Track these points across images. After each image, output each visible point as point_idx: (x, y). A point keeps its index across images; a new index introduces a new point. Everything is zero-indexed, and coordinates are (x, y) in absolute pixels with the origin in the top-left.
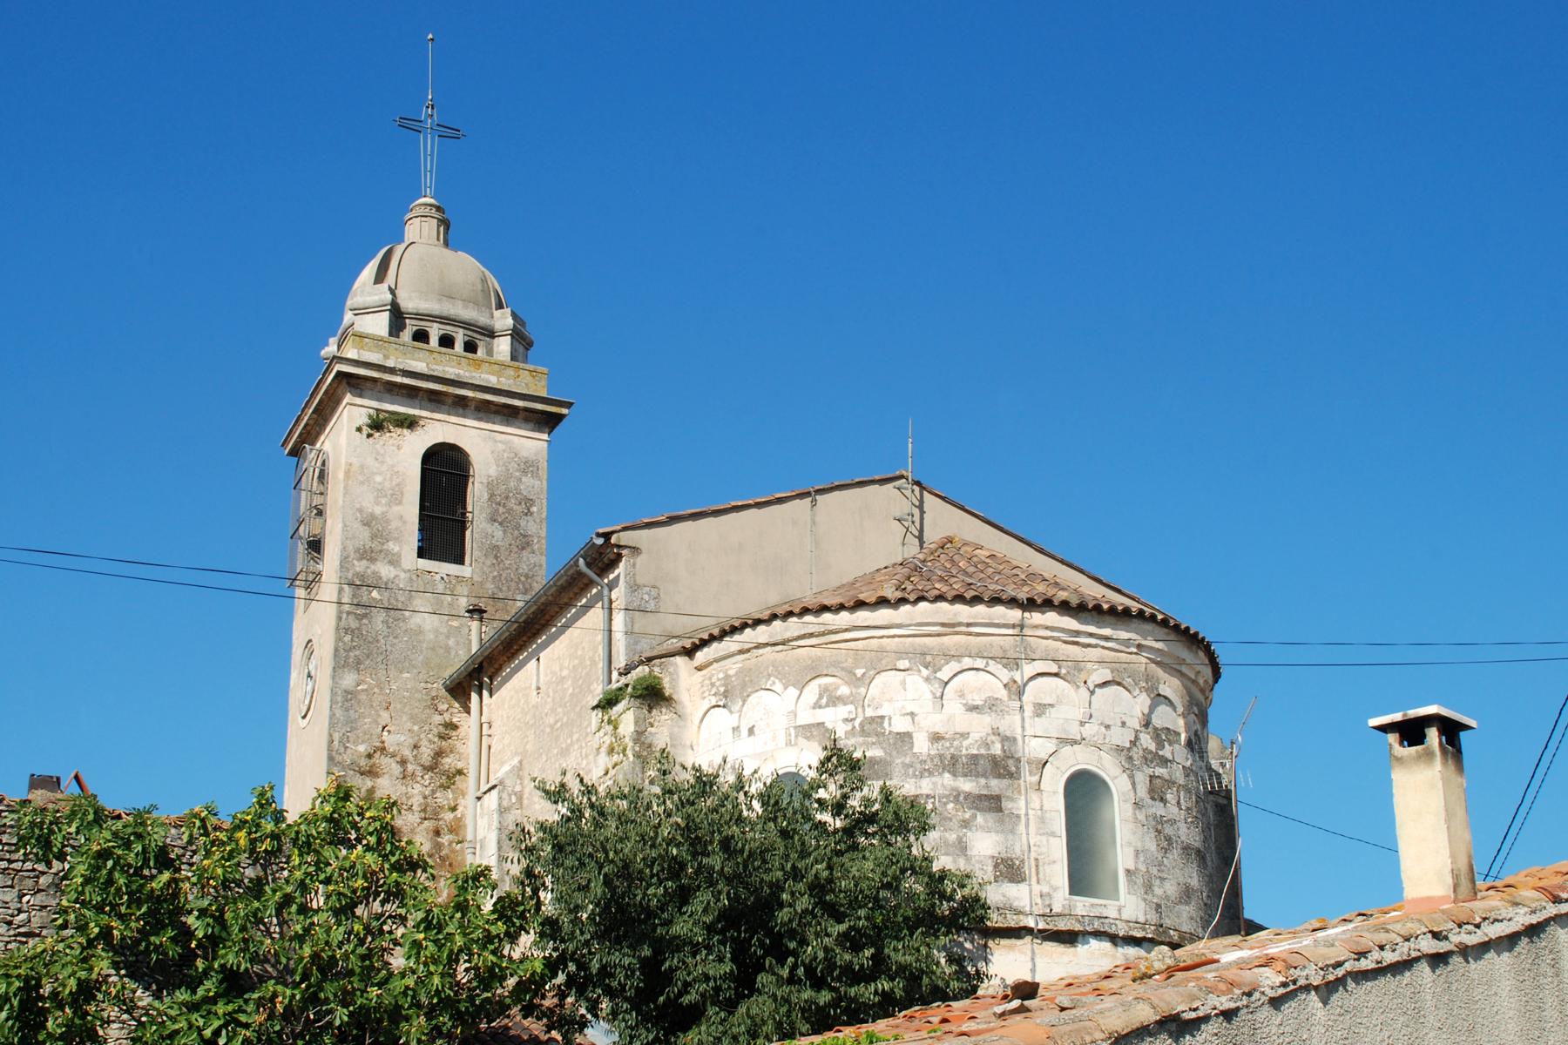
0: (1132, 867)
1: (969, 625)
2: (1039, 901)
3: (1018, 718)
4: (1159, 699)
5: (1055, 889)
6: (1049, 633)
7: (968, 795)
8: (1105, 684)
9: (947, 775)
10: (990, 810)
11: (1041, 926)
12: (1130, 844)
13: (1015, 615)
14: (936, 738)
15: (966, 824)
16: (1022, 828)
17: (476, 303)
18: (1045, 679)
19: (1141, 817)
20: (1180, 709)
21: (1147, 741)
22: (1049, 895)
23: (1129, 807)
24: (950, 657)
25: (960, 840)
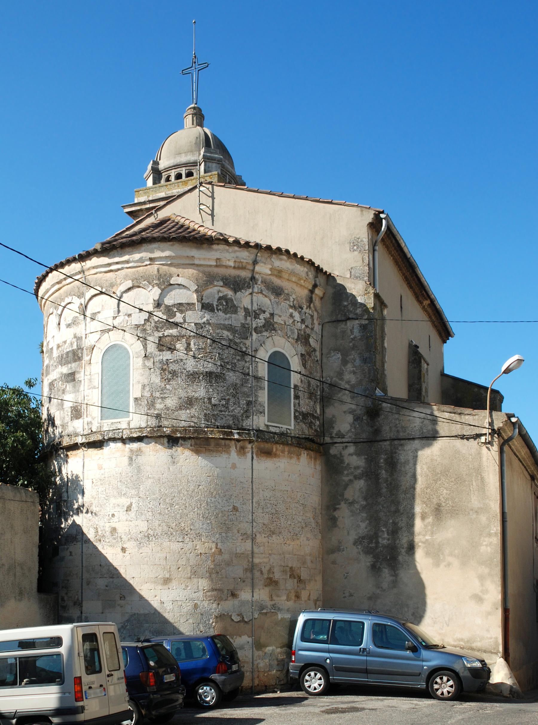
0: (139, 395)
2: (86, 427)
8: (129, 289)
12: (139, 382)
17: (191, 151)
19: (149, 364)
21: (160, 314)
22: (91, 422)
23: (140, 361)
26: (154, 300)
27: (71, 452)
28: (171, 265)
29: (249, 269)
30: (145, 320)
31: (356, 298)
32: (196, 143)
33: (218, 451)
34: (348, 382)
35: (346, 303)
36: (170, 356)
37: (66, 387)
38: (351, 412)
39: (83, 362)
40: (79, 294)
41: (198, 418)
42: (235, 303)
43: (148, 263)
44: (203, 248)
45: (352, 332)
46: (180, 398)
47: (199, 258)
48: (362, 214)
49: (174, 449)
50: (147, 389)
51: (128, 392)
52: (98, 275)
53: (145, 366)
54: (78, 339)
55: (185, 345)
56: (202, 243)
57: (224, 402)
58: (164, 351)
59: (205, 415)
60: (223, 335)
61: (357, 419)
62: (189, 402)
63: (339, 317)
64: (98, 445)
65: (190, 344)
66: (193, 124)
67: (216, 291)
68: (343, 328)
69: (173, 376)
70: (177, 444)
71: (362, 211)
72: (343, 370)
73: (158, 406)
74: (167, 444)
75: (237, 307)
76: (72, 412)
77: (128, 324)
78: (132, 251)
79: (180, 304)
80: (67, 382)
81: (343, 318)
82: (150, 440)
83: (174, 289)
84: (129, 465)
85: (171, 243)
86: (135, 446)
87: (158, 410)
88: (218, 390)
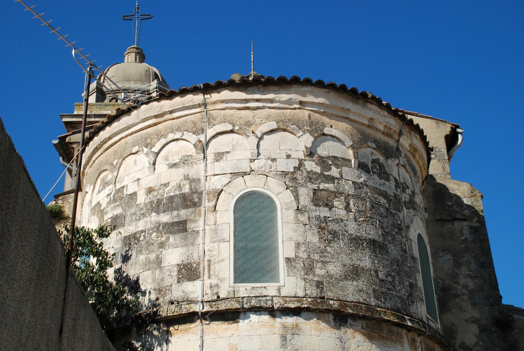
0: (292, 255)
1: (171, 112)
2: (209, 291)
3: (203, 165)
4: (320, 136)
5: (222, 280)
6: (224, 105)
7: (165, 225)
8: (272, 131)
9: (154, 214)
10: (179, 232)
11: (207, 308)
12: (291, 239)
13: (199, 98)
14: (150, 190)
15: (162, 245)
16: (200, 240)
18: (220, 137)
20: (349, 143)
22: (217, 286)
23: (291, 214)
24: (160, 136)
25: (158, 257)
26: (306, 148)
27: (176, 327)
28: (323, 114)
29: (394, 139)
30: (295, 168)
31: (461, 199)
32: (146, 75)
33: (392, 340)
34: (465, 287)
35: (450, 203)
36: (329, 213)
37: (168, 238)
38: (475, 321)
39: (202, 208)
40: (194, 130)
41: (367, 293)
42: (387, 170)
43: (298, 106)
44: (358, 103)
45: (462, 234)
46: (345, 266)
47: (354, 113)
48: (438, 126)
49: (343, 330)
50: (303, 248)
51: (276, 249)
52: (227, 110)
53: (299, 220)
54: (194, 181)
55: (345, 204)
56: (358, 99)
57: (390, 279)
58: (320, 206)
59: (374, 291)
60: (381, 201)
61: (483, 330)
62: (355, 272)
63: (444, 216)
64: (231, 316)
65: (349, 204)
66: (136, 61)
67: (369, 153)
68: (450, 228)
69: (334, 237)
70: (346, 324)
71: (437, 123)
72: (457, 273)
73: (318, 271)
74: (333, 323)
75: (389, 175)
76: (179, 272)
77: (273, 169)
79: (335, 157)
80: (171, 233)
81: (449, 218)
82: (310, 314)
84: (281, 347)
85: (327, 90)
86: (290, 320)
87: (319, 276)
88: (383, 263)
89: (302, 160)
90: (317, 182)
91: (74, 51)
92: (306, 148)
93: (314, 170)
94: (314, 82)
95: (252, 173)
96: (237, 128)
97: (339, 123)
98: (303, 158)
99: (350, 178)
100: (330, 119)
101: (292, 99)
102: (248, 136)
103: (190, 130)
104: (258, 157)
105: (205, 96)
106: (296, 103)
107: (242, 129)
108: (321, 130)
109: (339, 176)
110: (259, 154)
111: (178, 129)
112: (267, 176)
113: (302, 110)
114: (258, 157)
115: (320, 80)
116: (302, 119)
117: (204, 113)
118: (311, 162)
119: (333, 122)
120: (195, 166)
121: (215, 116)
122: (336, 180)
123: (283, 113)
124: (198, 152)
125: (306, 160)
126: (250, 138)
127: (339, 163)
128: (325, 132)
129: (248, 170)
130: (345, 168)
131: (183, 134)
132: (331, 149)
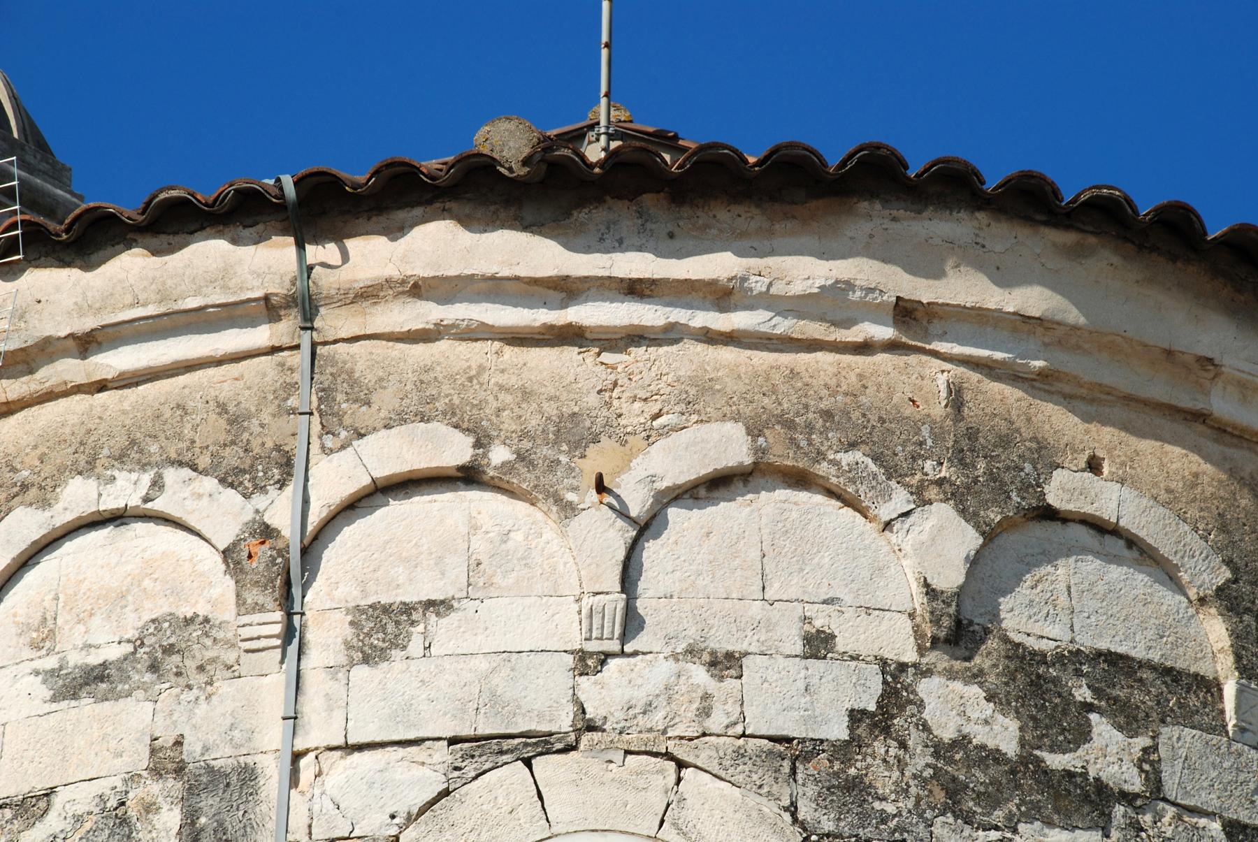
1: (87, 344)
3: (275, 683)
4: (1020, 524)
6: (426, 313)
8: (718, 485)
13: (268, 262)
18: (396, 509)
26: (931, 592)
28: (1041, 384)
30: (856, 716)
40: (232, 457)
43: (885, 332)
47: (1242, 385)
52: (443, 345)
77: (716, 722)
78: (771, 233)
79: (1112, 658)
83: (1069, 551)
85: (1069, 238)
89: (903, 667)
90: (998, 816)
91: (16, 135)
92: (931, 592)
93: (980, 736)
94: (991, 184)
95: (586, 738)
96: (499, 455)
97: (1147, 445)
98: (910, 656)
99: (1209, 800)
100: (1087, 419)
101: (850, 285)
102: (569, 510)
103: (204, 461)
104: (624, 638)
105: (310, 248)
106: (871, 312)
107: (531, 465)
108: (1025, 488)
109: (1135, 783)
110: (632, 623)
111: (130, 454)
112: (681, 765)
113: (913, 359)
114: (624, 638)
115: (1027, 176)
116: (909, 410)
117: (300, 359)
118: (957, 686)
119: (1103, 438)
120: (224, 687)
121: (369, 379)
122: (1119, 810)
123: (794, 374)
124: (252, 596)
125: (928, 673)
126: (579, 523)
127: (1138, 696)
128: (1052, 499)
129: (564, 722)
130: (1176, 731)
131: (158, 484)
132: (1094, 604)
